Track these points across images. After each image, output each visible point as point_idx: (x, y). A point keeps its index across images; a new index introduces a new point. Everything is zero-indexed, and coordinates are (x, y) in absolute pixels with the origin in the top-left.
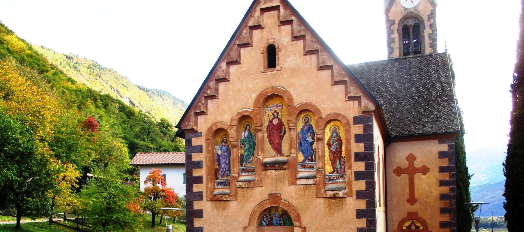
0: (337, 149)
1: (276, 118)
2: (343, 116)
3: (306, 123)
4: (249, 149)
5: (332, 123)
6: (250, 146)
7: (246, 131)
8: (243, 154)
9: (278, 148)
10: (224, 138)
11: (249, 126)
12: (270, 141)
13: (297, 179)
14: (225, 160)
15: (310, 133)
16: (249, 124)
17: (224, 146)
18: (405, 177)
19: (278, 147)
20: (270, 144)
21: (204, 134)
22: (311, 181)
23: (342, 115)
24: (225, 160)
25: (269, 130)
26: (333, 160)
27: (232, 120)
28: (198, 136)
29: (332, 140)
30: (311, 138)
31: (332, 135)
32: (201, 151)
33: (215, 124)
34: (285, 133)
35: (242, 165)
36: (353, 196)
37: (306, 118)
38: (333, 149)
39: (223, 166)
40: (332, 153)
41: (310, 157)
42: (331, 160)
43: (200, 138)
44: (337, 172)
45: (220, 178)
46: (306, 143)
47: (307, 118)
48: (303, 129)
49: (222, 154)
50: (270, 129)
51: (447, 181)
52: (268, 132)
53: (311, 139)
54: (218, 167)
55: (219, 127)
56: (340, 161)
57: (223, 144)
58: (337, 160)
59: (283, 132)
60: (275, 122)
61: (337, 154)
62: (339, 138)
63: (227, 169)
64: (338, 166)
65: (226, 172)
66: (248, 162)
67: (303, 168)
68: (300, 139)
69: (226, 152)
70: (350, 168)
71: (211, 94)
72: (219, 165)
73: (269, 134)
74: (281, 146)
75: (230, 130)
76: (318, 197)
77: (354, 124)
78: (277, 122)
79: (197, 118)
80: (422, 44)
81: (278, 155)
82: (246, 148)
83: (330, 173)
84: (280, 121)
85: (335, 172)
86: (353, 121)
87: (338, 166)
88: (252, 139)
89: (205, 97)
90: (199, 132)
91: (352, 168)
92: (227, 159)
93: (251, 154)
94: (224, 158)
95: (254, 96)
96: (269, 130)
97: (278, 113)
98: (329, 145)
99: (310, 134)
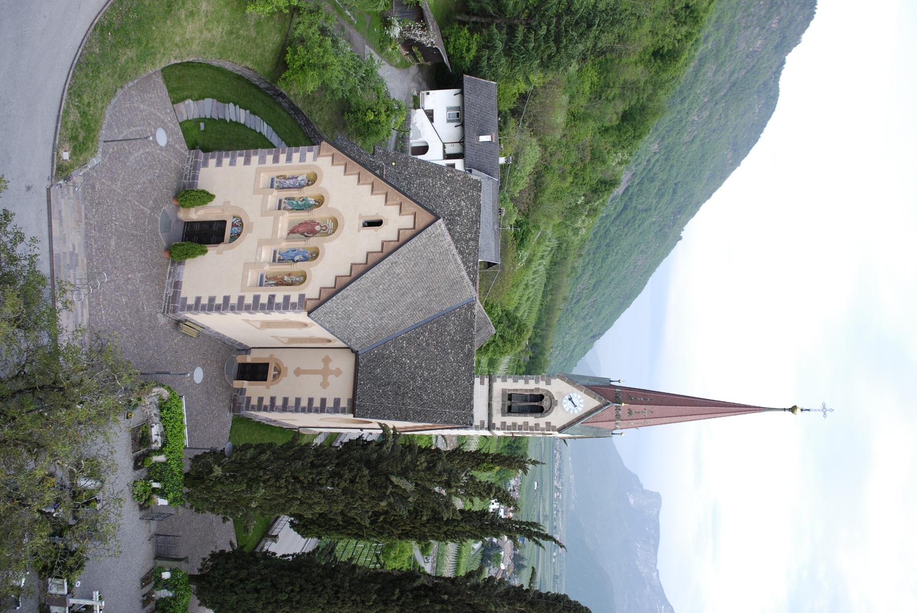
4: (299, 205)
7: (314, 202)
18: (320, 366)
19: (295, 231)
21: (315, 163)
28: (314, 157)
32: (300, 161)
35: (285, 199)
39: (287, 182)
51: (312, 405)
60: (317, 228)
63: (285, 186)
69: (299, 184)
74: (295, 233)
80: (517, 415)
82: (300, 202)
95: (339, 208)
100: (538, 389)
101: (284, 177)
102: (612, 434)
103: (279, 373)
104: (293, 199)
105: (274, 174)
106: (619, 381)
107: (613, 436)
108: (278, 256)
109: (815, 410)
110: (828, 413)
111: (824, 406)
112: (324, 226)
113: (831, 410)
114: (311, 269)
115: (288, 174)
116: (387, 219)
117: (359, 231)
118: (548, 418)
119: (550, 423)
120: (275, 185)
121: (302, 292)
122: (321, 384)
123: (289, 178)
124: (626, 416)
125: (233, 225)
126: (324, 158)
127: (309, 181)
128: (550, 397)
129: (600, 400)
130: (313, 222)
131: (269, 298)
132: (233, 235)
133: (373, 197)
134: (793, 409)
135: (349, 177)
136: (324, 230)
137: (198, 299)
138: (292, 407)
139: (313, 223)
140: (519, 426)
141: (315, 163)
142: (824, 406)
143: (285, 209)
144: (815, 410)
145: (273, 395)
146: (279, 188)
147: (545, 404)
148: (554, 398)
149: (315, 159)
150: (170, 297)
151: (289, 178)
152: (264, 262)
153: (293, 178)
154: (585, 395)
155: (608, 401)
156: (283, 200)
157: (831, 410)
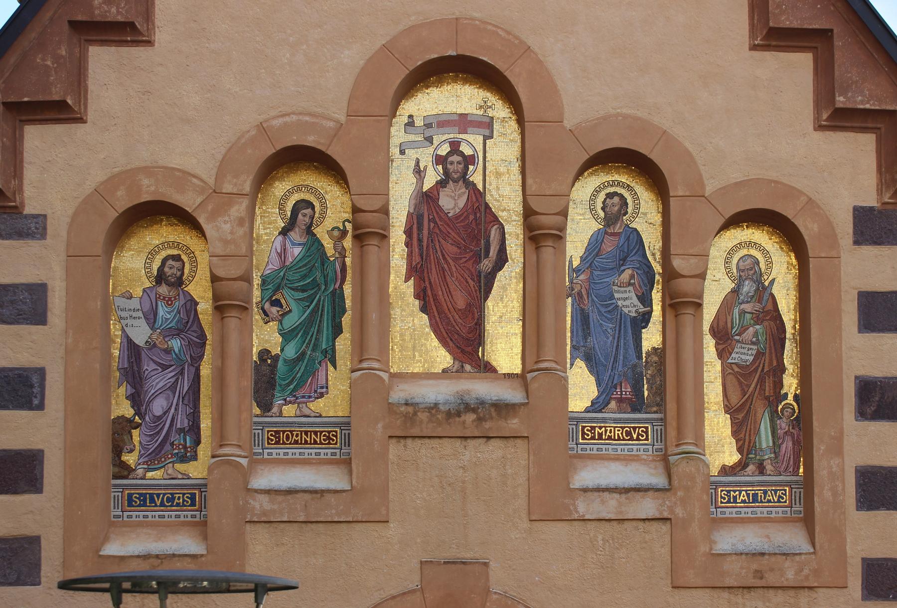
0: (759, 355)
1: (456, 181)
2: (803, 199)
3: (611, 219)
5: (759, 236)
6: (315, 311)
7: (296, 235)
8: (276, 351)
9: (464, 332)
10: (164, 261)
11: (308, 211)
12: (421, 294)
13: (249, 490)
14: (170, 374)
15: (629, 272)
16: (312, 199)
17: (169, 301)
20: (424, 309)
22: (647, 507)
23: (801, 193)
24: (170, 374)
25: (420, 240)
26: (739, 410)
27: (223, 168)
28: (22, 234)
29: (736, 311)
30: (633, 295)
31: (735, 292)
32: (39, 316)
33: (128, 177)
34: (502, 259)
36: (850, 584)
37: (610, 196)
38: (743, 355)
39: (158, 406)
40: (735, 374)
41: (627, 390)
42: (728, 409)
43: (31, 242)
44: (761, 470)
45: (140, 472)
46: (610, 320)
47: (616, 199)
48: (594, 247)
49: (151, 345)
50: (425, 232)
52: (416, 250)
53: (635, 301)
54: (127, 410)
55: (145, 198)
56: (774, 416)
57: (163, 289)
58: (760, 411)
59: (493, 252)
61: (761, 380)
62: (770, 307)
63: (182, 422)
64: (765, 439)
65: (175, 438)
66: (299, 393)
67: (277, 443)
68: (580, 294)
69: (177, 332)
70: (837, 449)
71: (120, 18)
72: (136, 399)
73: (417, 259)
75: (214, 216)
76: (681, 583)
77: (857, 242)
78: (462, 202)
79: (22, 136)
81: (461, 370)
82: (291, 321)
83: (725, 470)
84: (477, 196)
85: (751, 468)
86: (850, 230)
87: (765, 439)
88: (325, 277)
89: (77, 26)
90: (28, 210)
91: (847, 447)
92: (182, 373)
93: (318, 355)
94: (165, 367)
96: (420, 240)
97: (470, 160)
98: (721, 333)
99: (632, 277)
121: (845, 226)
126: (30, 174)
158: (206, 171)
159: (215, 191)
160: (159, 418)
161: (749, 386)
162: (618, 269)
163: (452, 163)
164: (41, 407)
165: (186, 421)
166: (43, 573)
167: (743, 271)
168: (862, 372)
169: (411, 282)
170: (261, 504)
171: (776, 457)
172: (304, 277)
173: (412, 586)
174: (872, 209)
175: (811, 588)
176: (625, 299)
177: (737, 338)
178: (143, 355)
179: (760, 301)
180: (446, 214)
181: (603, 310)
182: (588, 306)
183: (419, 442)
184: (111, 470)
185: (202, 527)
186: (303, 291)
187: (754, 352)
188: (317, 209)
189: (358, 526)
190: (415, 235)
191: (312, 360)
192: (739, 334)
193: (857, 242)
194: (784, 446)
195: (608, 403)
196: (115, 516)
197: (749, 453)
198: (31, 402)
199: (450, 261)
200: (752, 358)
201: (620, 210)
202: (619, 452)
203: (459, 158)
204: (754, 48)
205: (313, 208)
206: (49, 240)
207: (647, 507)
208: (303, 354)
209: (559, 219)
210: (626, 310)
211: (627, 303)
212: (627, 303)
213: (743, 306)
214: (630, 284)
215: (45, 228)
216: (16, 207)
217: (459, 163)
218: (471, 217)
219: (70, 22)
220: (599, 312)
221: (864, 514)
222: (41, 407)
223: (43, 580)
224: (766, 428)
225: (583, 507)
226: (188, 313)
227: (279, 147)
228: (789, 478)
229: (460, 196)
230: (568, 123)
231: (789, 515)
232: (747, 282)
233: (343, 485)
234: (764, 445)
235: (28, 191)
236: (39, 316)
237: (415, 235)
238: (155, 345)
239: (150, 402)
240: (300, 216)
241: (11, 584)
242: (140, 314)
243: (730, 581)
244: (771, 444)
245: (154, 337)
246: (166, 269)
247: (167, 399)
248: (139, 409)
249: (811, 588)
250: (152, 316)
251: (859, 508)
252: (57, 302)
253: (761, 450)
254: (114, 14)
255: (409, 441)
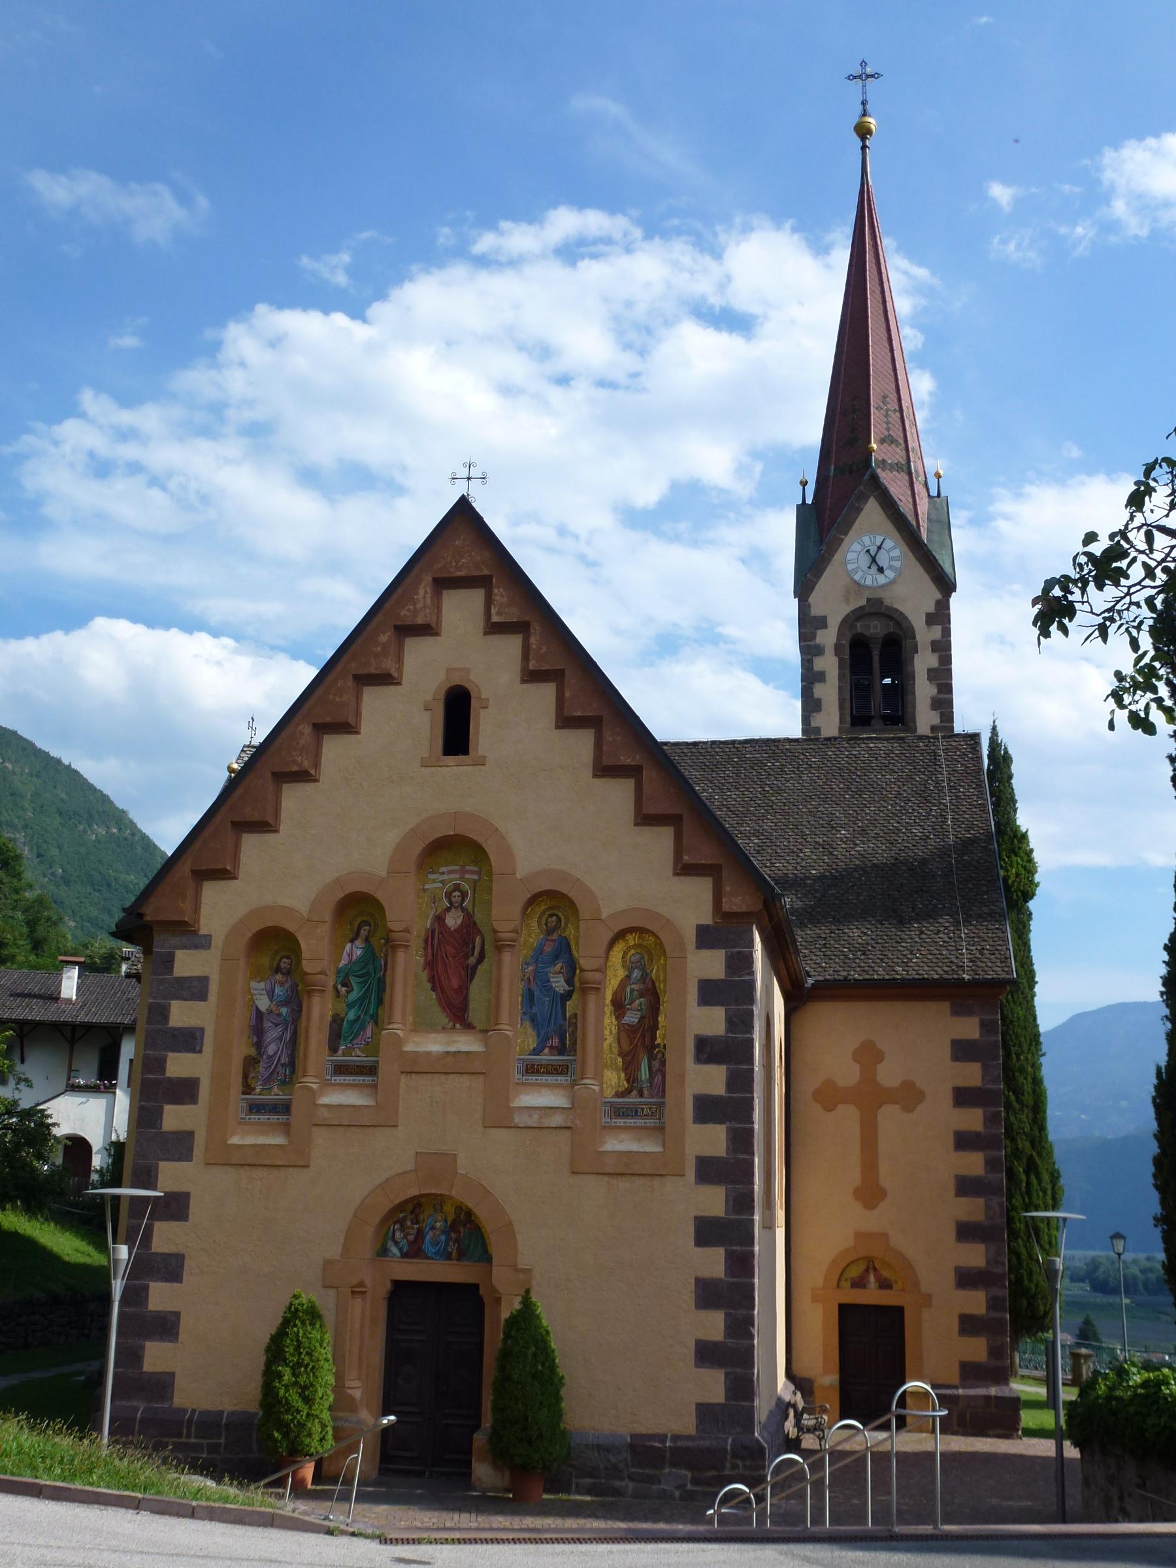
0: (642, 1018)
1: (456, 908)
6: (367, 990)
7: (358, 943)
14: (280, 1029)
17: (282, 984)
20: (433, 989)
21: (218, 942)
26: (627, 1055)
28: (196, 947)
29: (628, 990)
31: (628, 977)
32: (202, 996)
38: (631, 1018)
39: (271, 1050)
41: (555, 1041)
44: (641, 1094)
47: (554, 918)
49: (270, 1012)
53: (563, 983)
60: (453, 920)
62: (650, 986)
65: (280, 1070)
68: (529, 979)
69: (285, 1003)
77: (698, 947)
78: (459, 921)
81: (454, 1027)
82: (353, 996)
85: (634, 1093)
88: (375, 969)
94: (277, 1025)
95: (392, 837)
100: (838, 648)
101: (250, 1063)
102: (939, 495)
103: (871, 1265)
104: (337, 1020)
105: (236, 1100)
106: (804, 484)
107: (943, 494)
108: (546, 1057)
109: (864, 93)
110: (869, 70)
111: (855, 77)
112: (449, 895)
113: (864, 64)
114: (605, 913)
115: (241, 1049)
116: (448, 671)
117: (481, 762)
118: (918, 621)
119: (928, 615)
120: (276, 1094)
121: (690, 937)
122: (909, 1108)
123: (259, 1045)
124: (898, 450)
125: (414, 1251)
126: (204, 910)
127: (278, 970)
128: (858, 619)
129: (863, 499)
130: (429, 939)
131: (709, 1061)
132: (453, 1248)
133: (365, 727)
134: (863, 132)
135: (284, 815)
136: (464, 895)
137: (706, 1354)
138: (988, 1207)
139: (436, 936)
140: (939, 692)
141: (218, 942)
142: (855, 77)
143: (373, 1047)
144: (864, 93)
145: (951, 1277)
146: (292, 1068)
147: (876, 629)
148: (862, 608)
149: (203, 943)
150: (695, 1481)
151: (259, 1045)
152: (573, 1099)
153: (258, 1030)
154: (852, 533)
155: (866, 477)
156: (339, 1058)
157: (864, 64)
158: (303, 907)
159: (308, 920)
160: (272, 1056)
161: (635, 1038)
162: (553, 962)
163: (454, 897)
164: (200, 1051)
165: (287, 1059)
166: (194, 1154)
167: (633, 963)
168: (697, 1033)
169: (426, 971)
170: (324, 1113)
171: (651, 1086)
172: (362, 969)
173: (409, 1168)
174: (708, 926)
175: (661, 1175)
176: (557, 982)
177: (628, 1007)
178: (264, 1018)
179: (644, 983)
180: (449, 929)
181: (543, 989)
182: (534, 987)
183: (419, 1076)
184: (241, 1089)
185: (286, 1128)
186: (362, 977)
187: (639, 1016)
188: (372, 927)
189: (380, 1129)
190: (430, 942)
191: (364, 1021)
192: (630, 1005)
193: (698, 947)
194: (656, 1080)
195: (544, 1049)
196: (241, 1118)
197: (633, 1083)
198: (195, 1049)
199: (451, 959)
200: (637, 1020)
201: (556, 925)
202: (549, 1082)
203: (459, 894)
204: (636, 824)
205: (370, 925)
206: (212, 950)
207: (558, 1120)
208: (359, 1017)
209: (512, 935)
210: (557, 989)
211: (558, 984)
212: (558, 984)
213: (633, 986)
214: (560, 973)
215: (210, 944)
216: (194, 931)
217: (459, 896)
218: (465, 930)
219: (232, 822)
220: (541, 990)
221: (697, 1126)
222: (200, 1051)
223: (194, 1158)
224: (645, 1067)
225: (518, 1119)
226: (292, 991)
227: (347, 892)
228: (659, 1100)
229: (458, 917)
230: (518, 876)
231: (658, 1125)
232: (636, 971)
233: (371, 1102)
234: (643, 1078)
235: (203, 921)
236: (202, 996)
237: (430, 942)
238: (272, 1012)
239: (267, 1046)
240: (362, 931)
241: (176, 1161)
242: (264, 992)
243: (608, 1169)
244: (648, 1076)
245: (272, 1006)
246: (282, 964)
247: (277, 1045)
248: (260, 1051)
249: (661, 1175)
250: (271, 993)
251: (694, 1122)
252: (214, 987)
253: (641, 1080)
254: (256, 817)
255: (413, 1075)
